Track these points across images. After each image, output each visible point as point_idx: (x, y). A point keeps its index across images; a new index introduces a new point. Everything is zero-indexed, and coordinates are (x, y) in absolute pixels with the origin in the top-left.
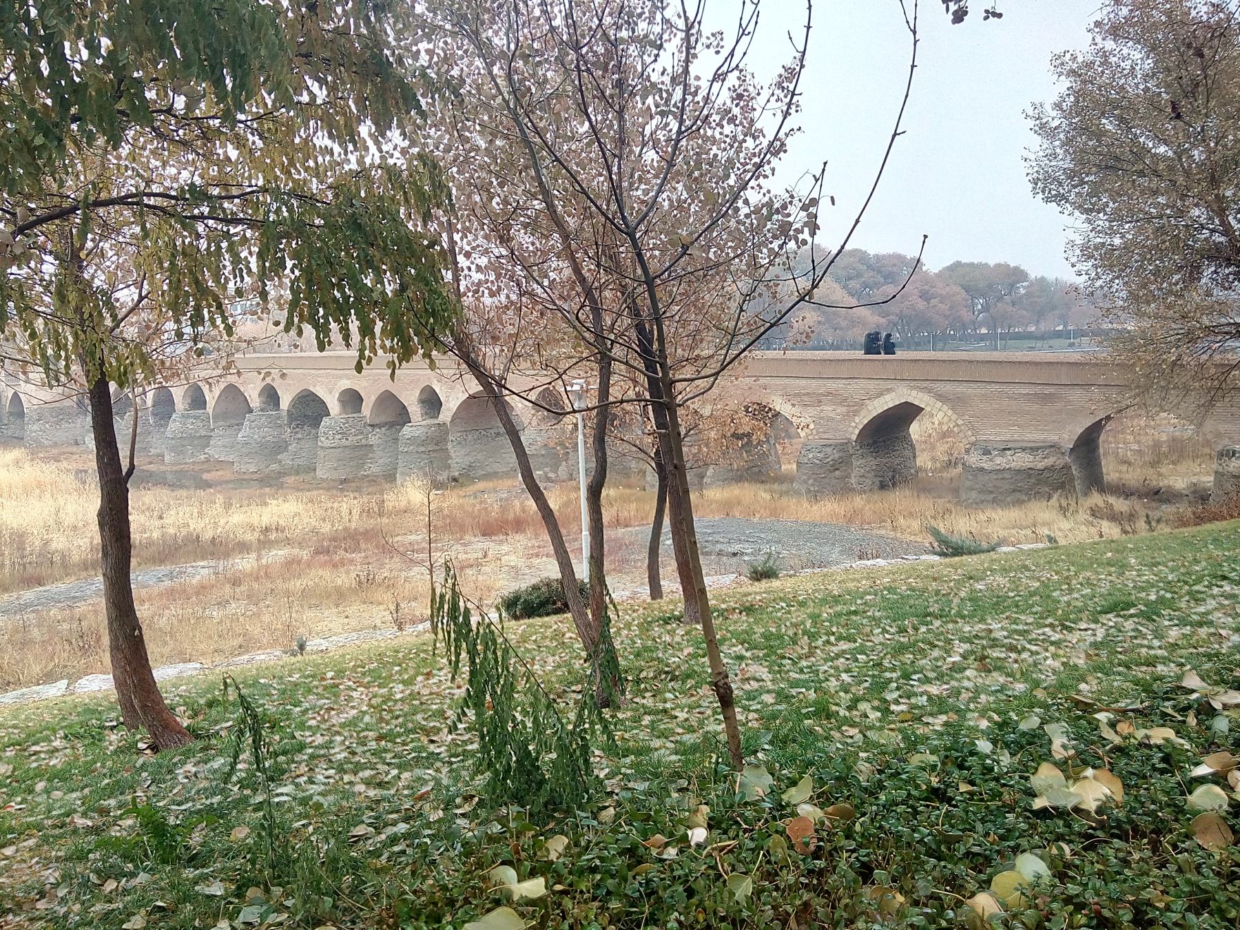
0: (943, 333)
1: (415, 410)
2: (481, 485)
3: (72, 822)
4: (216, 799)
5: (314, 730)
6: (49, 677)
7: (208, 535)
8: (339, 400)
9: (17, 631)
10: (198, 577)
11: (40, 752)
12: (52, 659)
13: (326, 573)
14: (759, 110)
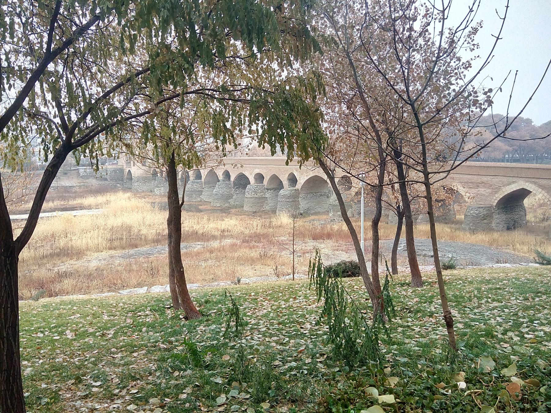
0: (542, 155)
1: (285, 183)
2: (312, 217)
3: (159, 345)
4: (215, 342)
5: (251, 317)
6: (140, 285)
7: (201, 232)
8: (254, 178)
9: (127, 265)
10: (197, 249)
11: (142, 315)
12: (140, 277)
13: (247, 251)
14: (459, 48)
